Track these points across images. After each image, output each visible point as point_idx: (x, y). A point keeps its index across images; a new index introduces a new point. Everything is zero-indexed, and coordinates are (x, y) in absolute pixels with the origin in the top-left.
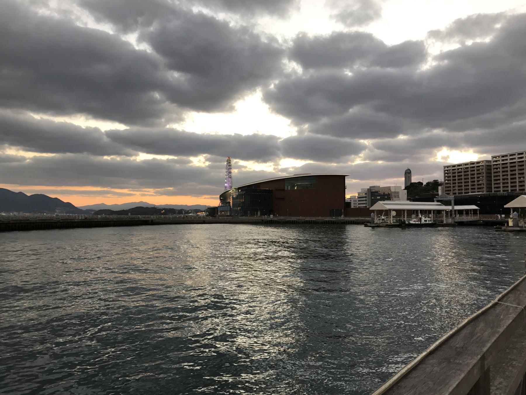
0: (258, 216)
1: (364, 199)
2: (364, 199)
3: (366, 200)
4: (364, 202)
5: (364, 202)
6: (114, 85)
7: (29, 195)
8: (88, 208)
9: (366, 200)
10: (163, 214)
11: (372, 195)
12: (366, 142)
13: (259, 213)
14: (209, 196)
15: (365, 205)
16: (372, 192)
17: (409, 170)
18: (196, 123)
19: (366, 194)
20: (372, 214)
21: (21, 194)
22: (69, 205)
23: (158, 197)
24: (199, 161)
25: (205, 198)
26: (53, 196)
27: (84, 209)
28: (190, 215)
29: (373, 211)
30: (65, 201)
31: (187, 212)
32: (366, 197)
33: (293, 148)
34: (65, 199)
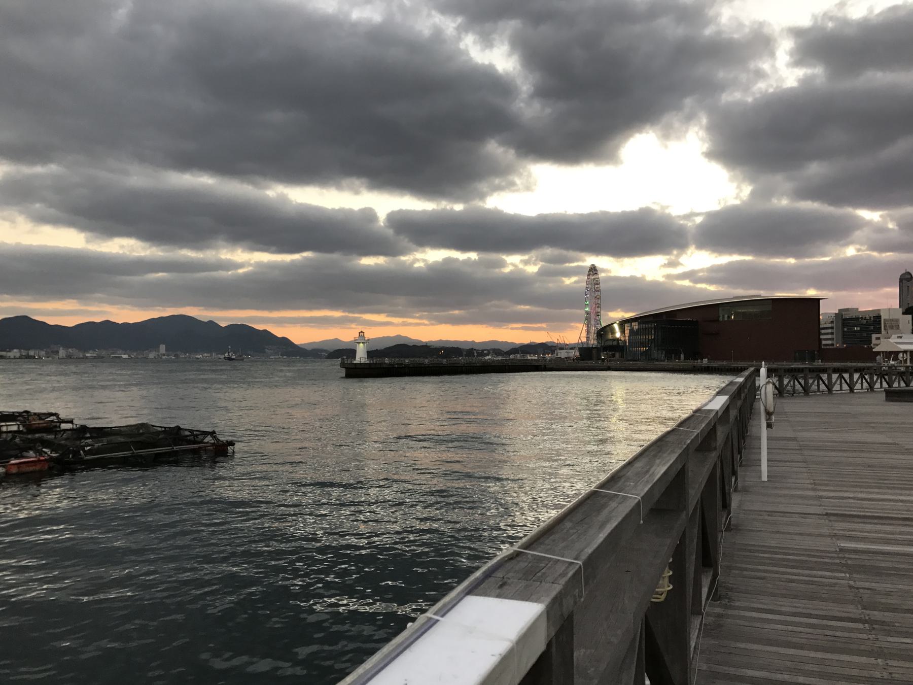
0: (682, 361)
1: (830, 331)
2: (830, 331)
3: (832, 334)
4: (829, 336)
5: (829, 336)
6: (412, 122)
7: (223, 324)
8: (315, 347)
9: (832, 334)
10: (443, 357)
11: (844, 325)
12: (870, 215)
13: (682, 356)
14: (520, 325)
15: (830, 342)
16: (844, 320)
17: (909, 273)
18: (545, 190)
19: (832, 322)
20: (878, 357)
21: (211, 325)
22: (285, 341)
23: (431, 327)
24: (514, 262)
25: (512, 329)
26: (260, 327)
27: (309, 348)
28: (487, 358)
29: (878, 353)
30: (279, 336)
31: (482, 353)
32: (832, 328)
33: (722, 231)
34: (279, 332)
